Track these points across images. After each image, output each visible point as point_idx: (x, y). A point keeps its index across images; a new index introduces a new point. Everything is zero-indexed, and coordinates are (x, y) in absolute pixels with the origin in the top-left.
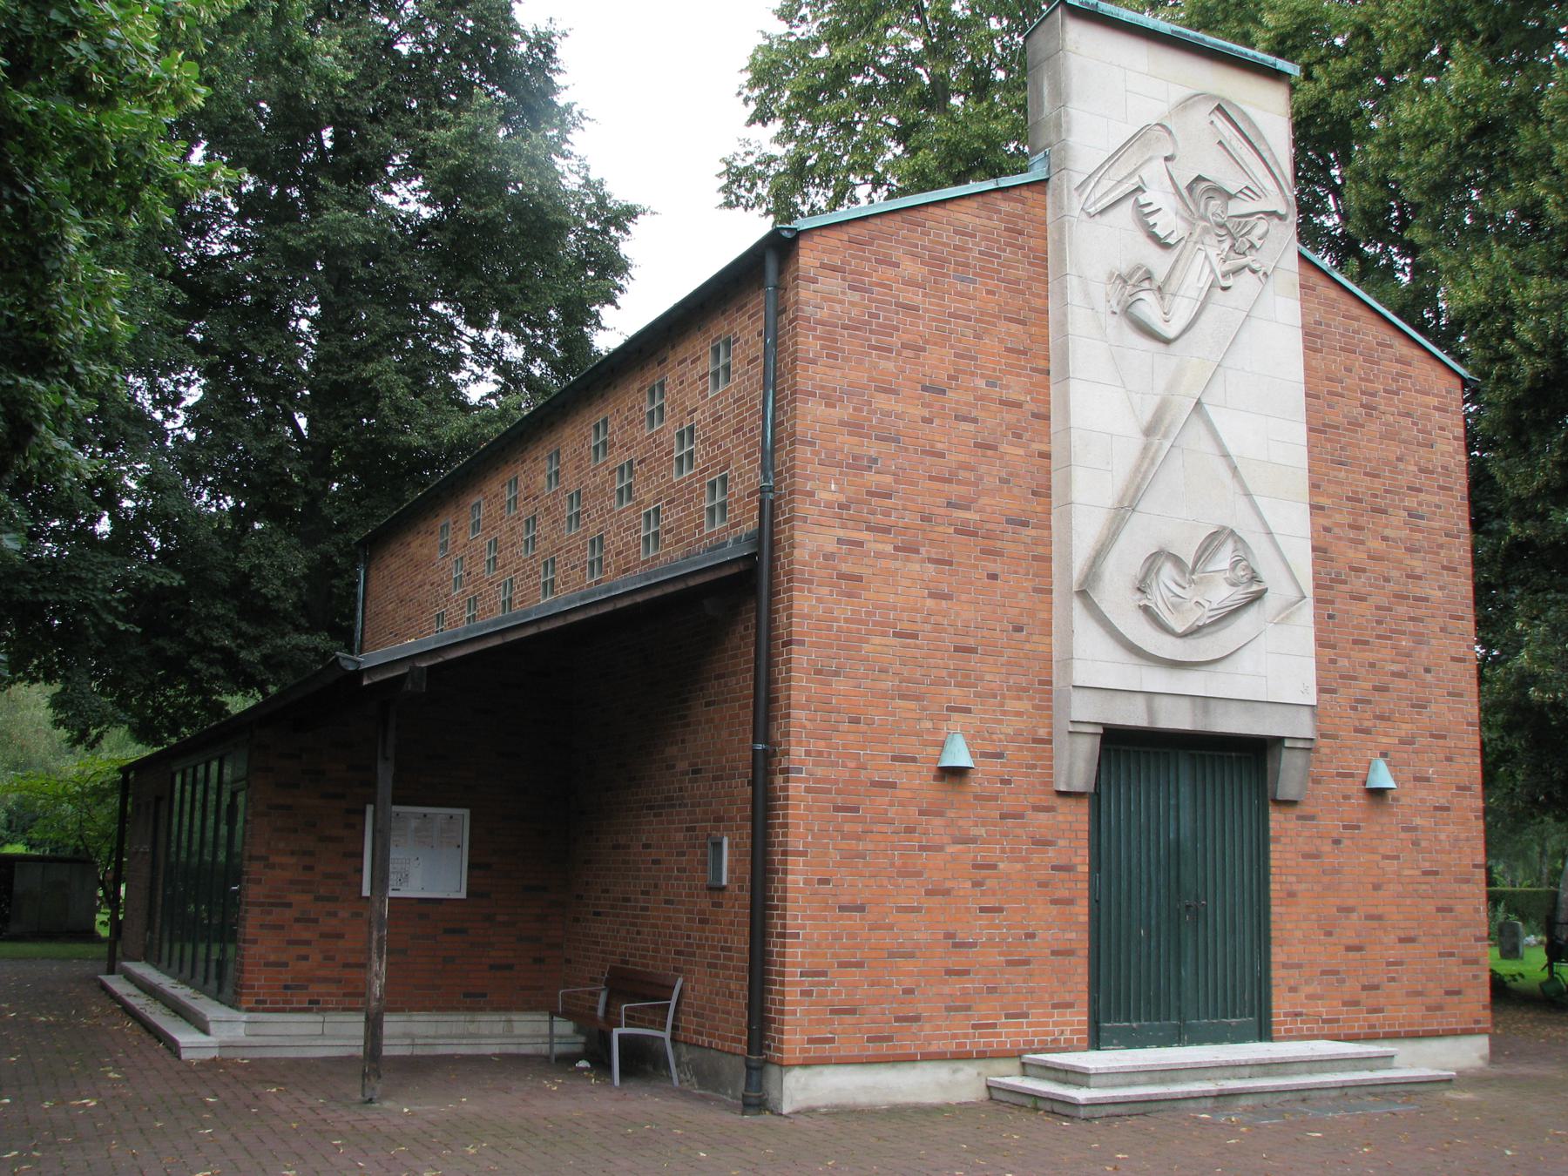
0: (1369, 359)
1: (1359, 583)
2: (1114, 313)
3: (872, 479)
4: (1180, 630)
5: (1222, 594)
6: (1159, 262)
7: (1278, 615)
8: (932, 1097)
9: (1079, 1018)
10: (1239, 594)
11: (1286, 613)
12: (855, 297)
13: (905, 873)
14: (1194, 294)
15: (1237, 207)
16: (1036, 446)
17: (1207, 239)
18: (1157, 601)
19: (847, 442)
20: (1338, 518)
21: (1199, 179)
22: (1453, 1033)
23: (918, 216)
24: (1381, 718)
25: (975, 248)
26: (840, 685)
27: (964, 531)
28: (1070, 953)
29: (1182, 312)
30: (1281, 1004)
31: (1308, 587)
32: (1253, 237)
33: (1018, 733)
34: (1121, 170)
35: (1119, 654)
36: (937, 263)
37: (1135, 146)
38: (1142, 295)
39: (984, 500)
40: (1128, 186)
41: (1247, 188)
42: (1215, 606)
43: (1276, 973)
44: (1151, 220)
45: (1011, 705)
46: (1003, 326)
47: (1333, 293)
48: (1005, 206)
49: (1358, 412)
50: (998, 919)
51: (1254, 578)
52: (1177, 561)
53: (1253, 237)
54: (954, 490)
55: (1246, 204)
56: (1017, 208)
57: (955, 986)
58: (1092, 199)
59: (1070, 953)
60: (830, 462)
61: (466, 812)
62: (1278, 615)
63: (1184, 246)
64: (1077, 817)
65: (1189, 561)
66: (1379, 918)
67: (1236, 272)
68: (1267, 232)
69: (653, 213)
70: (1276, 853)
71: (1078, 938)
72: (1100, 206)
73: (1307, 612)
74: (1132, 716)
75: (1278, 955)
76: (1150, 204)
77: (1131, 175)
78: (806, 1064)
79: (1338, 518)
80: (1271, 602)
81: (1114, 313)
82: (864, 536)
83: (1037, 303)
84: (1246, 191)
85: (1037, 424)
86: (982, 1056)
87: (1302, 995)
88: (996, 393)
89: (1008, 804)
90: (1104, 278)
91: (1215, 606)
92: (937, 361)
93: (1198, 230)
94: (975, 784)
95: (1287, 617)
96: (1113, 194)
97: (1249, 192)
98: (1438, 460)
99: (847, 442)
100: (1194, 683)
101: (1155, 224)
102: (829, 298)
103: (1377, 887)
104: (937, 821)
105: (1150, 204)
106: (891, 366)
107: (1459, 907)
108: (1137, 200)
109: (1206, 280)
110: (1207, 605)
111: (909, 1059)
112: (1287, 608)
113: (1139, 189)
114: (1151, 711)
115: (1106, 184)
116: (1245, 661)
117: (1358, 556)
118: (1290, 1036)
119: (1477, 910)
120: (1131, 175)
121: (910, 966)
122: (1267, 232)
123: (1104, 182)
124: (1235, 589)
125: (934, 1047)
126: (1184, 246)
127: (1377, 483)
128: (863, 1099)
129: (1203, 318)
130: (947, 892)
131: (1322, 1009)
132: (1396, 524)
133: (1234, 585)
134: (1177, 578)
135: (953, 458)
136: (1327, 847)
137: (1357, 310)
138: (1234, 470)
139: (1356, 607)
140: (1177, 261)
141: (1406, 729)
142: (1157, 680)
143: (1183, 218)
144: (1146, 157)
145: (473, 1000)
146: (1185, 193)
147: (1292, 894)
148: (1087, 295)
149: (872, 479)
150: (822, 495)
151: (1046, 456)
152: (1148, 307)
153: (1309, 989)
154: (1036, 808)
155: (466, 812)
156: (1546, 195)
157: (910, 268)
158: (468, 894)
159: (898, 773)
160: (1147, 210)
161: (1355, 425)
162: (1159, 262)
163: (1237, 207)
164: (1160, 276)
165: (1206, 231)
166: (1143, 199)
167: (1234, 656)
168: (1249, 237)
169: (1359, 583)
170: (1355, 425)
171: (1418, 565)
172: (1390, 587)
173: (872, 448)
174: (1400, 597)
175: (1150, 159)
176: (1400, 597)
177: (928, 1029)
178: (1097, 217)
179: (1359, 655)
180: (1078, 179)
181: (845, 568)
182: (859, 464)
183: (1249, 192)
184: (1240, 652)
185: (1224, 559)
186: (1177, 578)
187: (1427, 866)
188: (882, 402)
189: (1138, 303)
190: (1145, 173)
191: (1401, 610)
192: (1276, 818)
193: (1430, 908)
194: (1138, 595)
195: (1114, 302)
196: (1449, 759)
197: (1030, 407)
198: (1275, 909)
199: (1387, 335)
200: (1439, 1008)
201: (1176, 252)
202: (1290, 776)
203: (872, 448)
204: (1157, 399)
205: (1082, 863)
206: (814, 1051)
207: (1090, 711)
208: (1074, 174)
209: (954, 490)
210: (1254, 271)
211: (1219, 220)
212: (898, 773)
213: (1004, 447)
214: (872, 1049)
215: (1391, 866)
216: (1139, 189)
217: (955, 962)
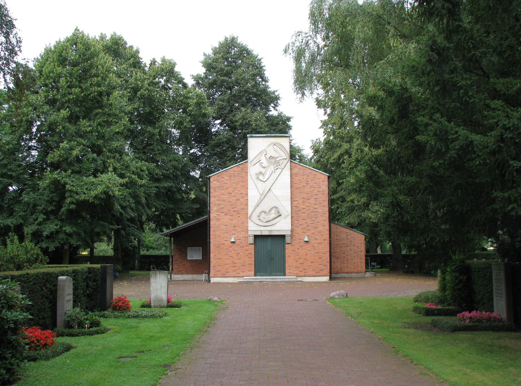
1: (304, 211)
5: (273, 216)
6: (263, 170)
10: (276, 216)
11: (286, 217)
12: (218, 183)
15: (277, 159)
16: (246, 199)
18: (261, 218)
19: (217, 202)
20: (300, 201)
22: (322, 276)
23: (228, 171)
24: (308, 230)
26: (217, 232)
28: (251, 264)
29: (266, 177)
30: (287, 271)
32: (280, 163)
33: (243, 236)
34: (257, 158)
35: (256, 225)
36: (230, 176)
39: (237, 207)
43: (286, 267)
45: (242, 233)
46: (240, 183)
48: (241, 166)
49: (305, 184)
50: (240, 260)
51: (279, 213)
52: (265, 212)
53: (280, 163)
54: (233, 206)
56: (243, 166)
57: (234, 268)
59: (251, 264)
60: (215, 205)
64: (253, 247)
65: (267, 212)
66: (307, 259)
74: (259, 233)
75: (287, 265)
79: (300, 201)
80: (283, 216)
82: (220, 214)
83: (246, 179)
85: (246, 196)
86: (238, 277)
87: (291, 270)
88: (239, 192)
89: (241, 245)
92: (230, 190)
94: (237, 243)
98: (321, 190)
99: (217, 202)
100: (269, 228)
103: (306, 255)
104: (231, 248)
106: (224, 191)
107: (323, 258)
111: (228, 277)
114: (261, 233)
115: (255, 161)
116: (278, 225)
117: (304, 207)
118: (289, 276)
119: (327, 258)
121: (228, 266)
125: (231, 276)
127: (308, 195)
128: (221, 282)
130: (233, 257)
131: (295, 272)
132: (312, 201)
135: (232, 202)
136: (296, 249)
137: (305, 169)
139: (303, 214)
141: (313, 232)
145: (187, 273)
148: (251, 177)
149: (221, 206)
150: (214, 209)
152: (261, 177)
153: (293, 269)
154: (246, 246)
156: (298, 159)
157: (226, 178)
159: (226, 243)
161: (304, 186)
162: (263, 170)
163: (277, 159)
164: (263, 173)
165: (271, 164)
166: (260, 162)
169: (304, 211)
170: (304, 186)
171: (316, 207)
172: (311, 210)
177: (230, 273)
179: (303, 221)
181: (217, 218)
182: (219, 205)
185: (273, 211)
187: (317, 252)
188: (222, 196)
190: (261, 158)
191: (313, 214)
192: (286, 245)
193: (317, 258)
196: (322, 236)
197: (245, 193)
199: (312, 171)
200: (319, 272)
202: (288, 240)
204: (263, 190)
206: (214, 275)
207: (252, 233)
209: (233, 206)
212: (226, 243)
214: (222, 276)
215: (309, 252)
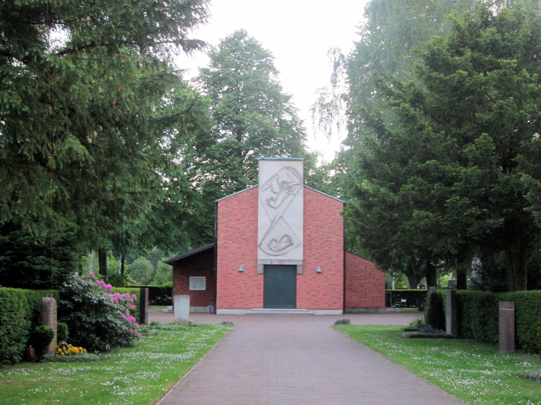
0: (322, 203)
1: (317, 240)
3: (229, 233)
5: (284, 245)
6: (274, 196)
8: (238, 313)
9: (262, 304)
11: (298, 246)
13: (234, 285)
18: (271, 247)
22: (334, 309)
25: (246, 198)
26: (224, 261)
27: (243, 239)
29: (278, 203)
30: (298, 304)
31: (302, 242)
36: (240, 202)
46: (250, 209)
47: (315, 193)
51: (290, 241)
61: (205, 277)
67: (289, 195)
69: (339, 127)
70: (298, 282)
71: (262, 294)
73: (302, 246)
74: (269, 263)
78: (220, 308)
80: (294, 245)
86: (246, 308)
97: (292, 182)
102: (223, 210)
109: (283, 197)
114: (271, 262)
137: (319, 195)
138: (289, 226)
139: (316, 244)
141: (326, 262)
142: (272, 258)
147: (301, 288)
149: (229, 233)
151: (257, 227)
152: (272, 203)
155: (205, 277)
157: (235, 203)
158: (206, 289)
161: (318, 214)
162: (274, 196)
169: (317, 240)
171: (331, 235)
173: (229, 229)
174: (326, 241)
176: (326, 241)
182: (227, 232)
183: (292, 182)
188: (231, 223)
191: (327, 243)
192: (298, 276)
198: (297, 290)
202: (299, 270)
203: (229, 229)
205: (262, 283)
207: (260, 263)
213: (250, 227)
217: (242, 296)
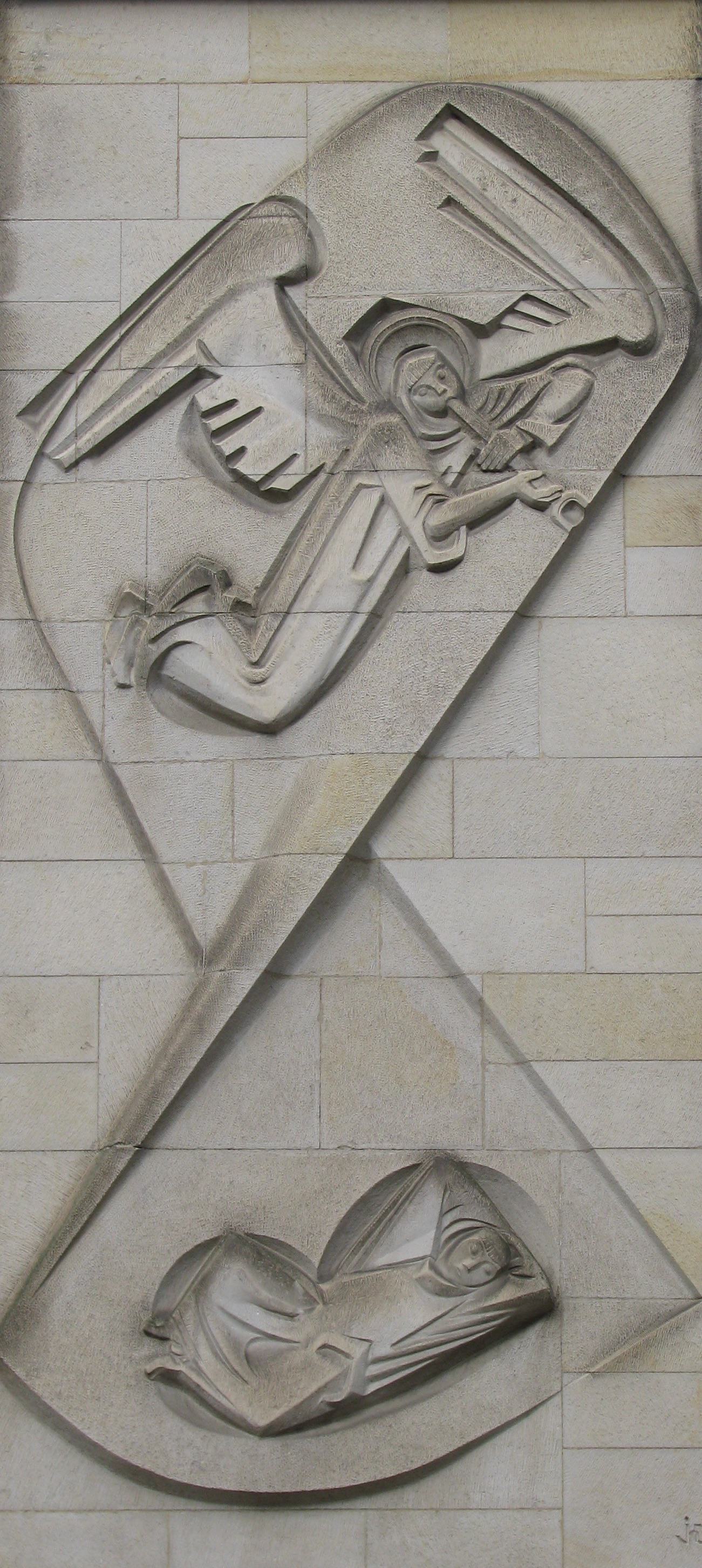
2: (123, 686)
4: (262, 1419)
7: (606, 1352)
14: (345, 600)
17: (387, 459)
21: (386, 307)
37: (199, 269)
38: (183, 633)
40: (167, 376)
41: (527, 298)
42: (386, 1350)
44: (228, 445)
55: (521, 340)
58: (69, 426)
62: (606, 1352)
63: (327, 482)
68: (586, 395)
72: (87, 441)
76: (231, 404)
77: (176, 345)
81: (123, 686)
84: (525, 307)
90: (101, 608)
91: (384, 1350)
93: (362, 440)
95: (636, 1354)
96: (126, 403)
101: (242, 451)
105: (231, 404)
108: (193, 403)
110: (358, 1351)
112: (639, 1331)
113: (198, 376)
115: (110, 380)
120: (176, 345)
122: (586, 395)
123: (103, 377)
124: (448, 1303)
126: (327, 482)
129: (372, 654)
133: (444, 1292)
134: (265, 1295)
140: (301, 526)
143: (322, 418)
144: (218, 293)
146: (340, 353)
160: (216, 422)
165: (385, 437)
166: (206, 397)
167: (458, 1468)
168: (526, 424)
175: (233, 294)
178: (87, 467)
180: (29, 389)
184: (487, 1448)
186: (265, 1295)
189: (177, 653)
194: (149, 1347)
195: (118, 664)
201: (300, 506)
204: (244, 871)
208: (20, 379)
210: (540, 507)
211: (430, 400)
216: (198, 376)
